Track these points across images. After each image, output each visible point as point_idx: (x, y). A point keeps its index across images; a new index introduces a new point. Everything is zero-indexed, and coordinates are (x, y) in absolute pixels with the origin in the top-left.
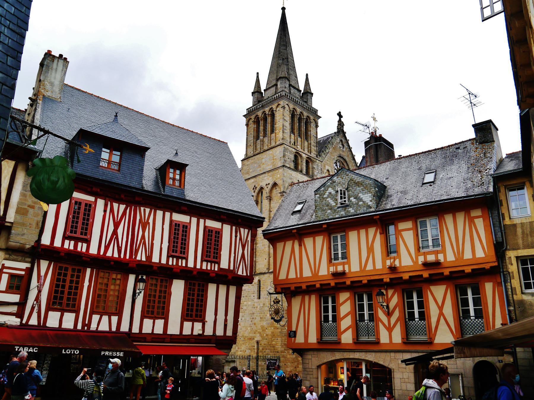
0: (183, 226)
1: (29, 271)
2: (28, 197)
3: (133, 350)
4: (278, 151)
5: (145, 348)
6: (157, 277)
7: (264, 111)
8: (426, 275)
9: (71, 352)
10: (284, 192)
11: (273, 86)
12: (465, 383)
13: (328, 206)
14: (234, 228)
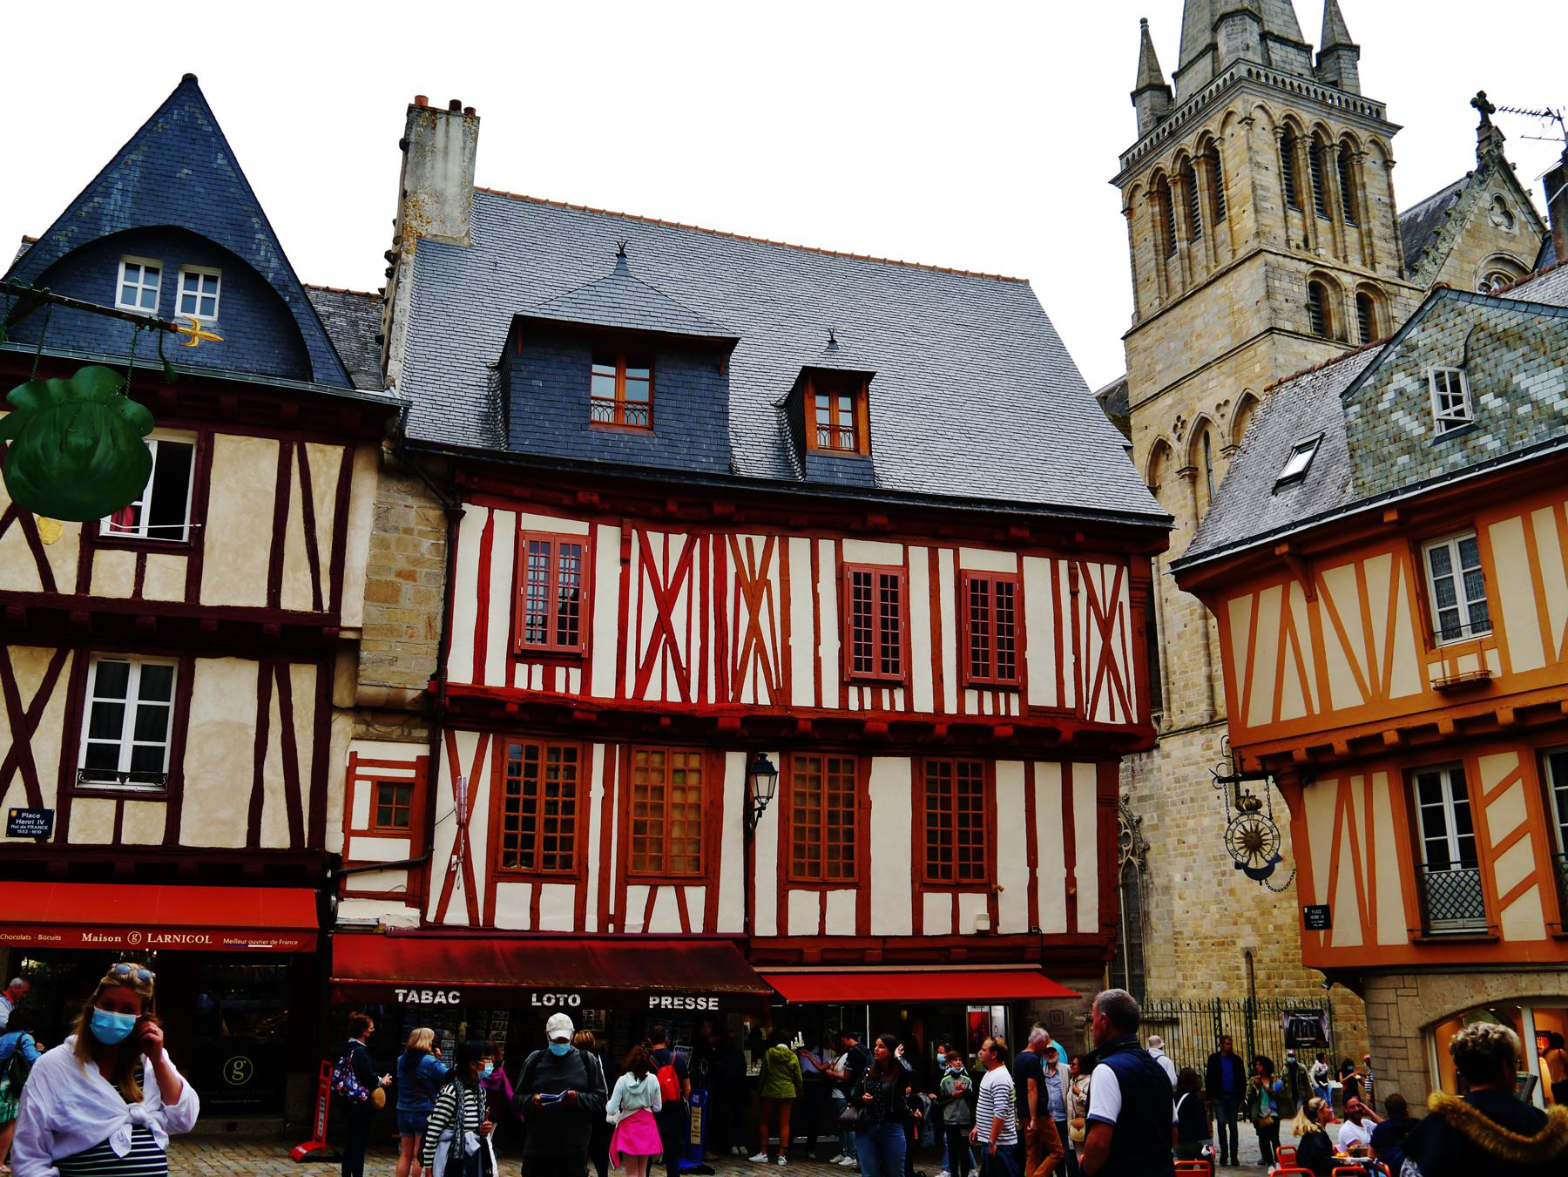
0: (884, 578)
1: (428, 767)
2: (393, 547)
3: (750, 989)
4: (1248, 281)
5: (799, 985)
6: (821, 753)
7: (1182, 150)
9: (558, 1000)
11: (1202, 54)
13: (1396, 439)
14: (1063, 565)
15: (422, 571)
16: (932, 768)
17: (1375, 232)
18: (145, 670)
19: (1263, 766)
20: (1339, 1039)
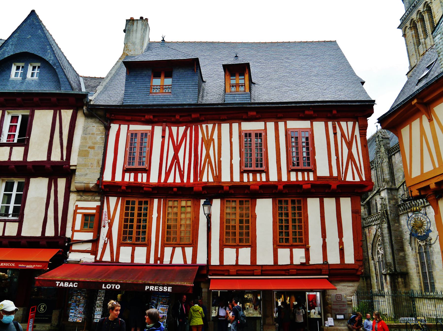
1: (100, 209)
2: (88, 139)
9: (112, 286)
15: (96, 146)
16: (280, 202)
18: (19, 183)
19: (420, 192)
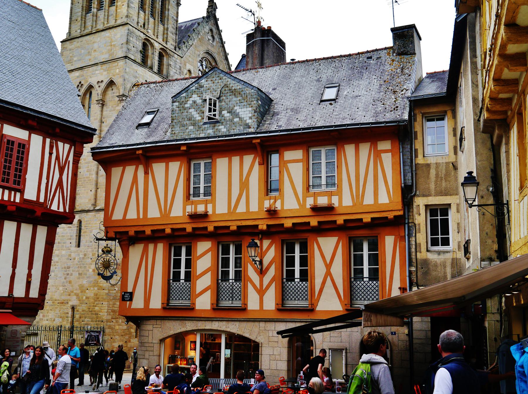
4: (120, 34)
8: (314, 222)
10: (123, 95)
12: (349, 360)
14: (48, 140)
17: (169, 29)
19: (116, 235)
20: (105, 342)
